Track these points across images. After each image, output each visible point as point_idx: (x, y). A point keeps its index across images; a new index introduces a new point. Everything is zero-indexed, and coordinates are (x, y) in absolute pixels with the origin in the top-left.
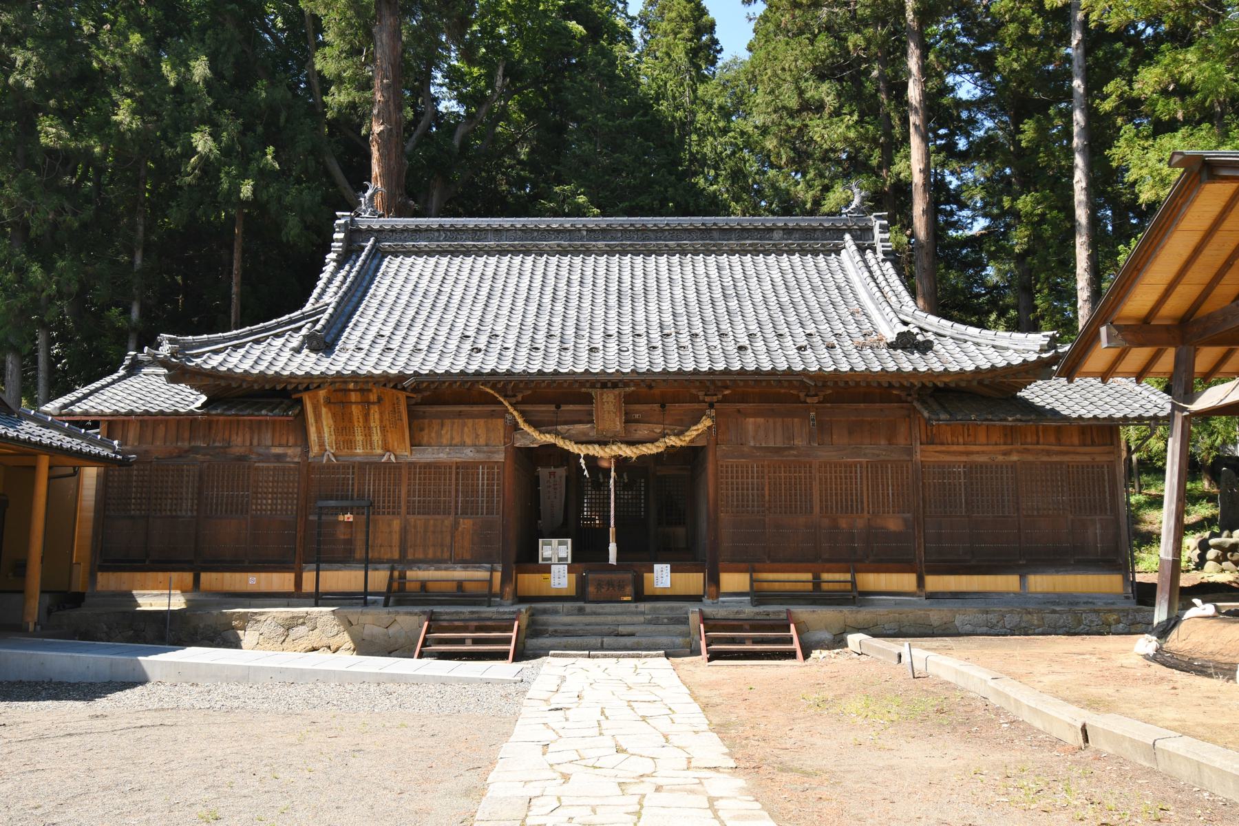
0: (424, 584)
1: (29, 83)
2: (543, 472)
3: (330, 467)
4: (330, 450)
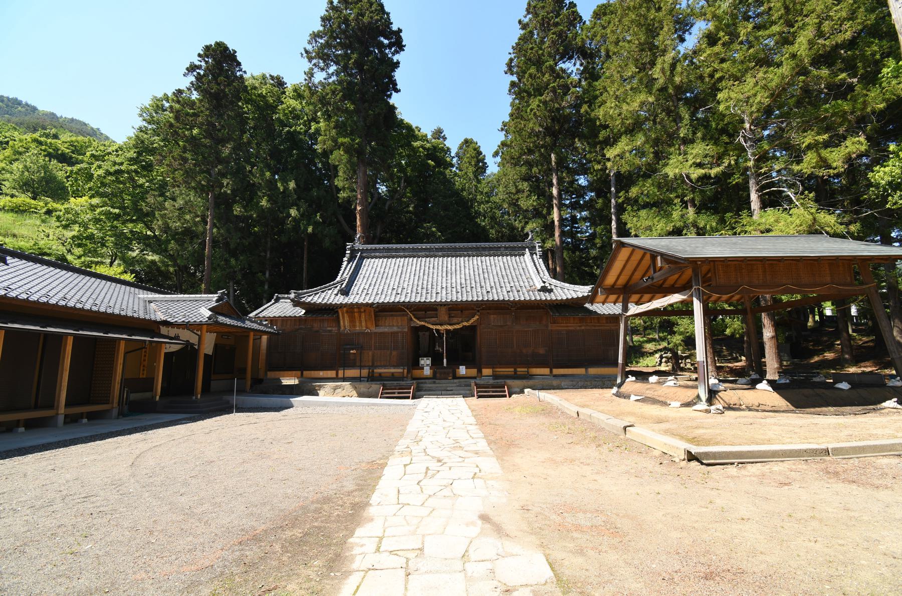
0: (380, 374)
1: (229, 192)
2: (421, 334)
3: (347, 334)
4: (348, 328)
